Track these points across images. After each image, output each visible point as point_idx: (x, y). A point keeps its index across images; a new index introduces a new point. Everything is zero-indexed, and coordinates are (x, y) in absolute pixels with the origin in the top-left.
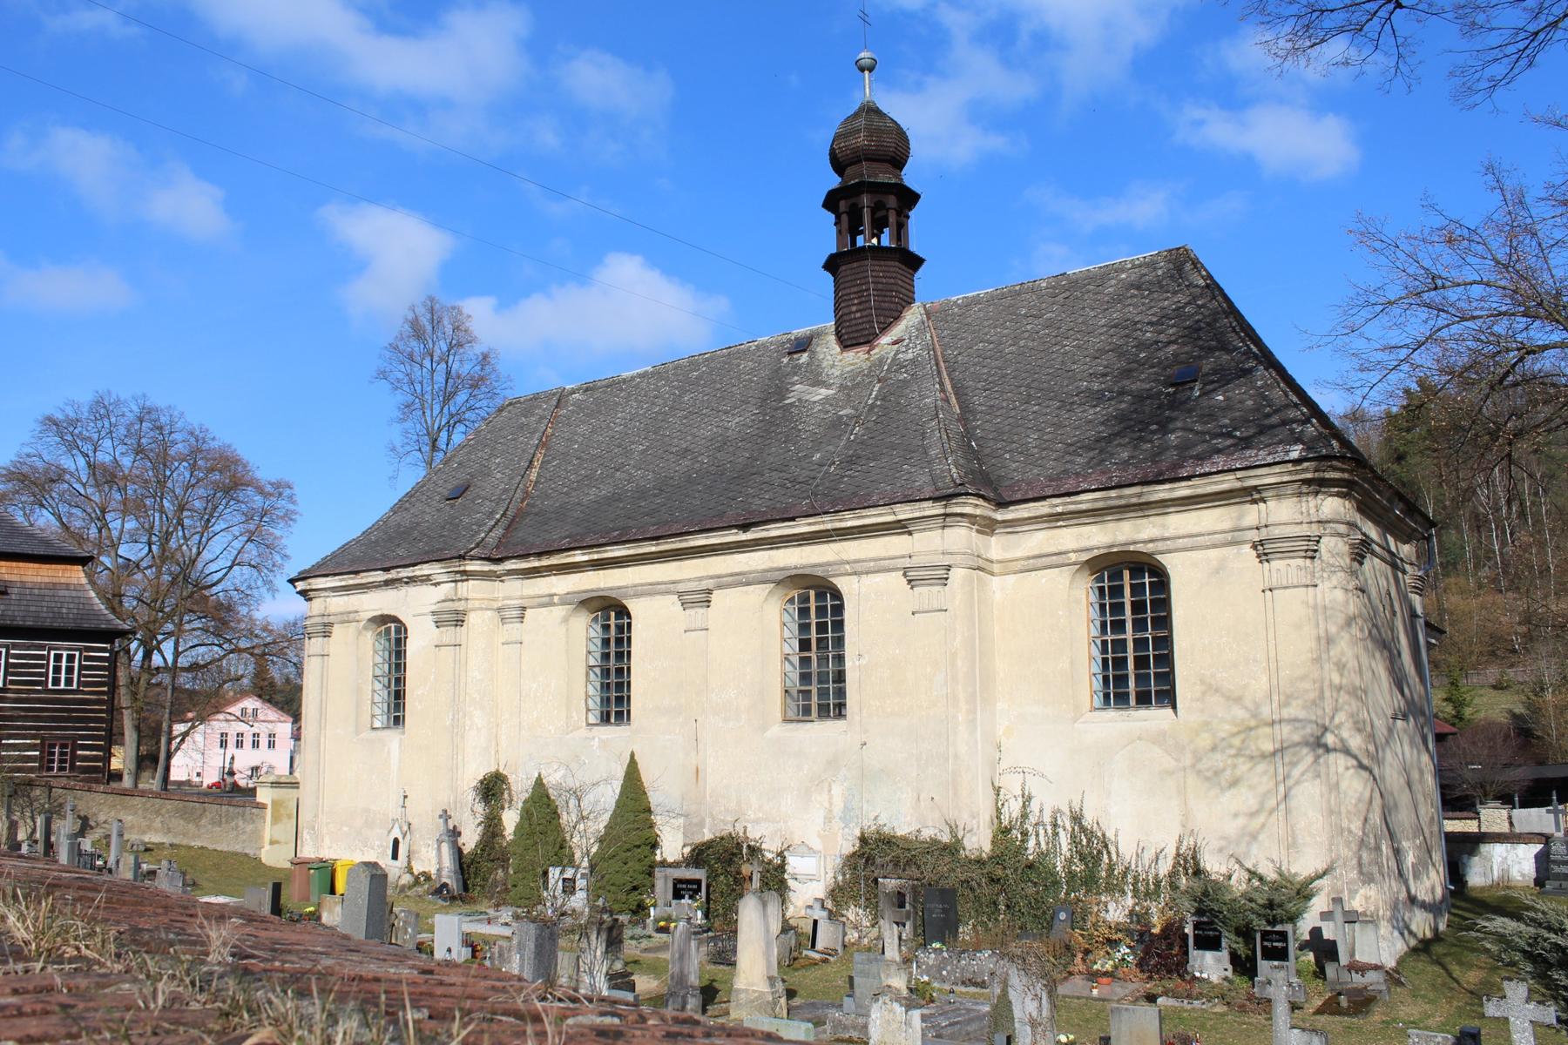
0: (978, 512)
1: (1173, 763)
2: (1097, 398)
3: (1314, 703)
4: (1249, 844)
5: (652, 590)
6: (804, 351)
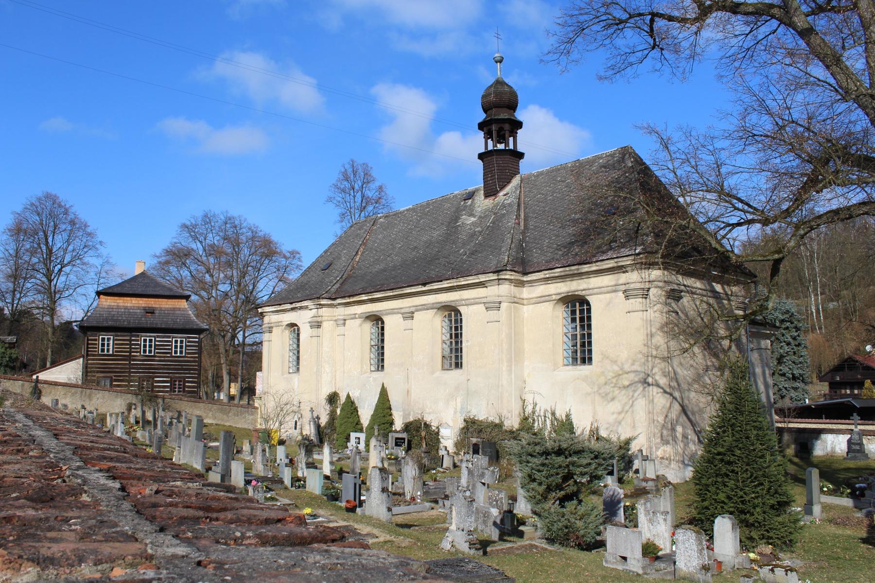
1: (590, 390)
2: (575, 222)
3: (644, 364)
4: (618, 426)
5: (392, 312)
6: (470, 199)
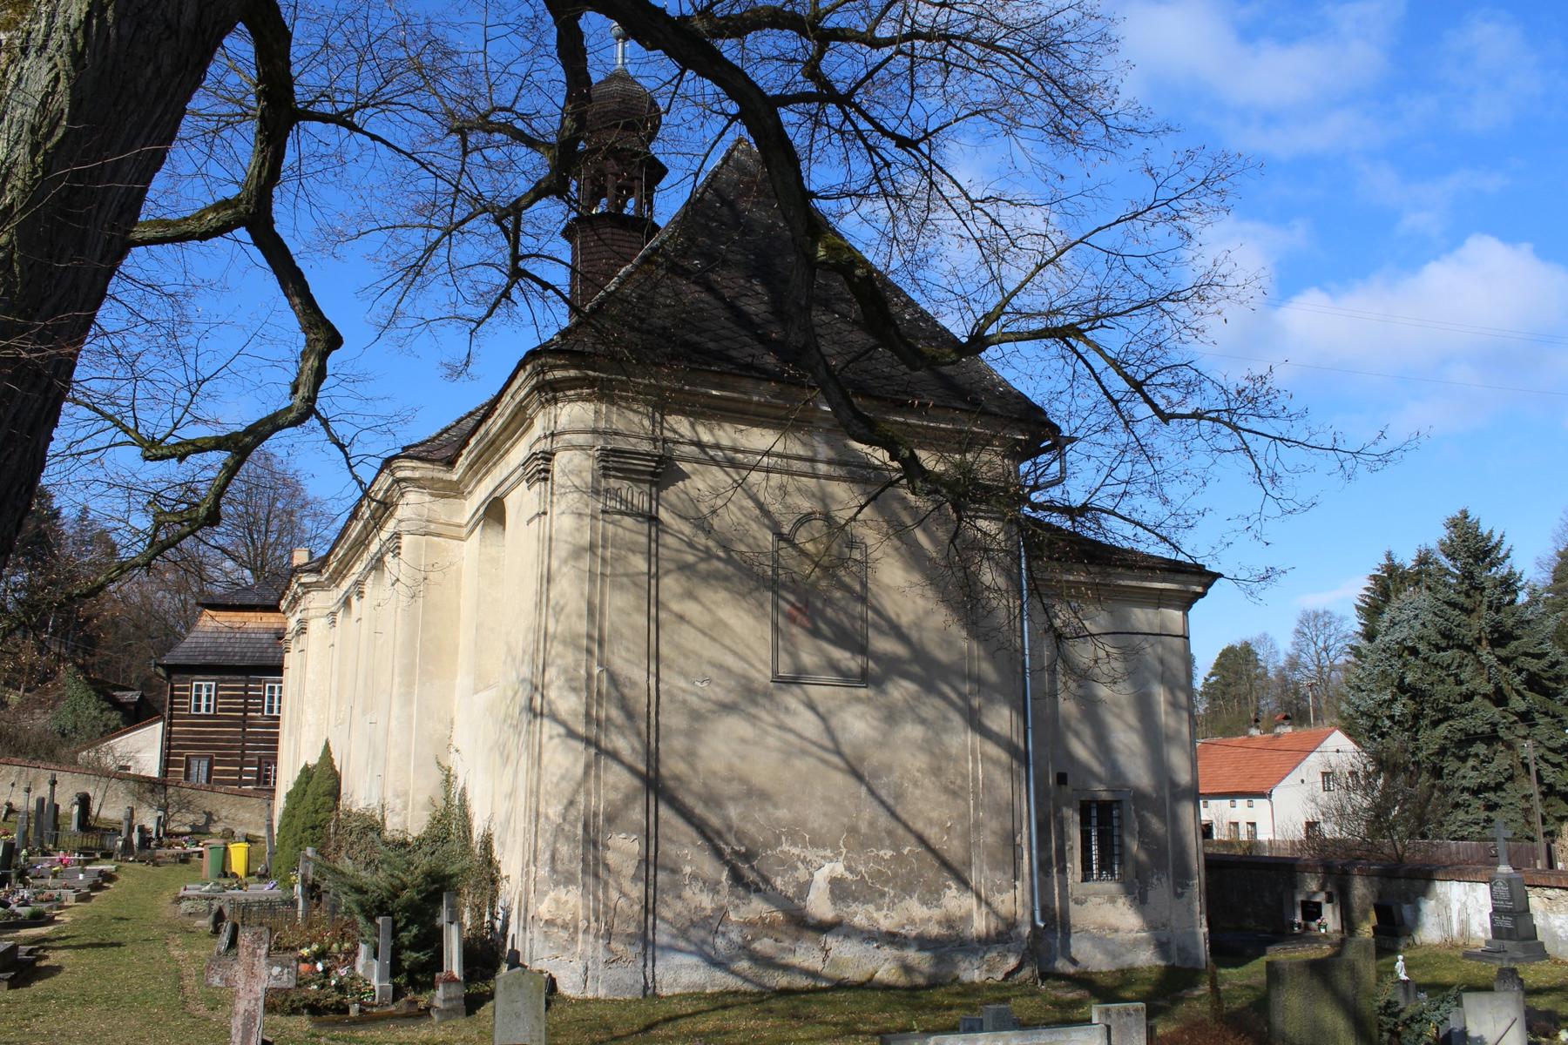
0: (417, 474)
